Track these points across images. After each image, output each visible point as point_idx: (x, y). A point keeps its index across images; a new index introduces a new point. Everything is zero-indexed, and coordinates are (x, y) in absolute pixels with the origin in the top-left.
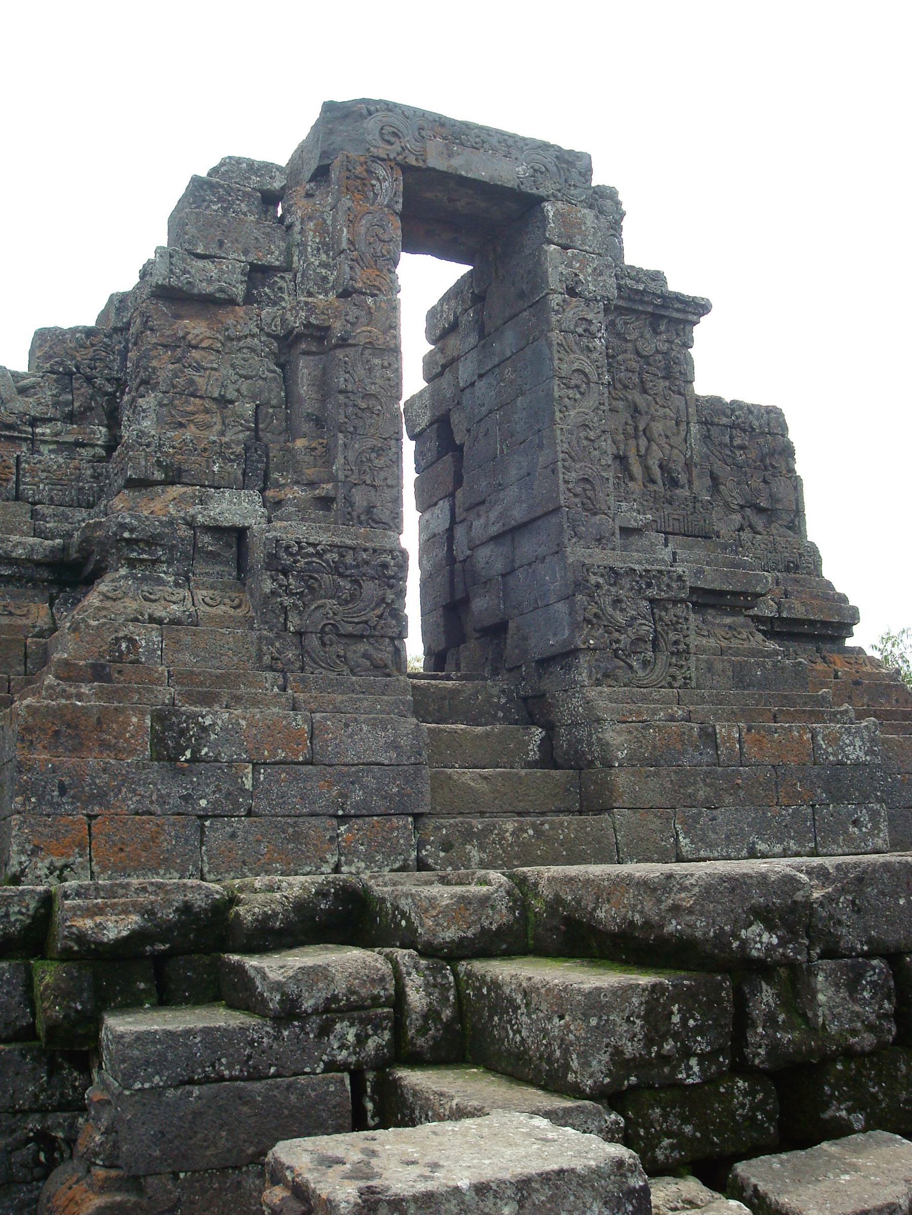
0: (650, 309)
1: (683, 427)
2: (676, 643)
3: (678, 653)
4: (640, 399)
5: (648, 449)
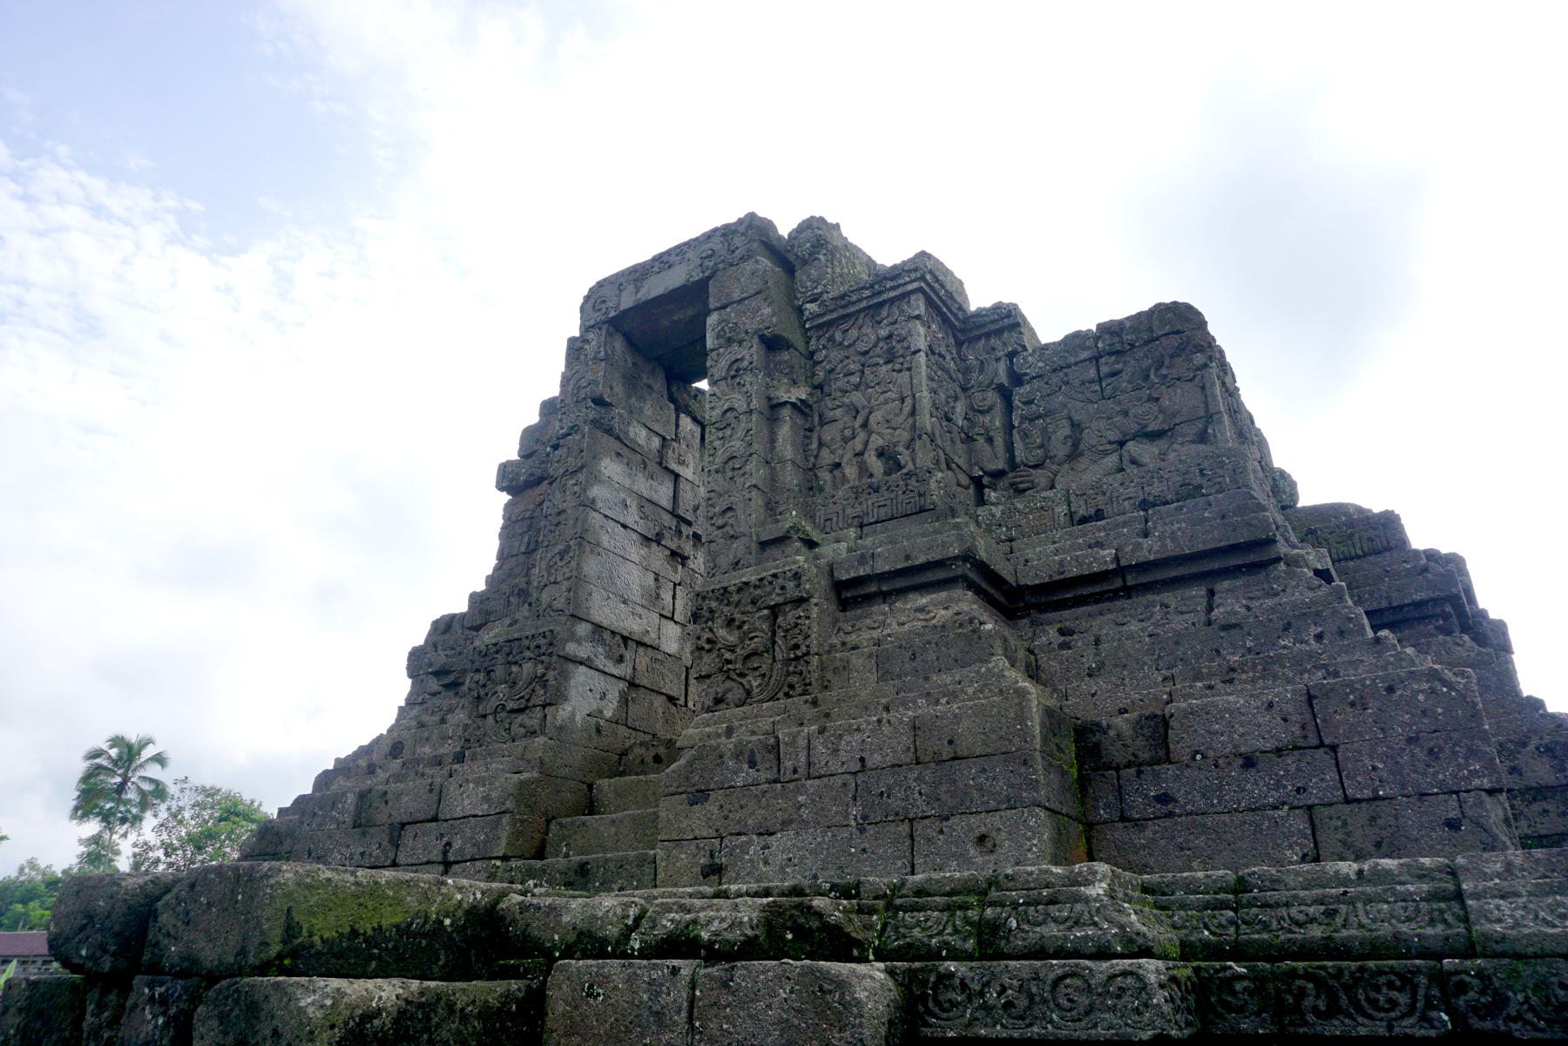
0: (864, 304)
1: (909, 401)
2: (797, 647)
3: (797, 658)
4: (856, 398)
5: (866, 444)
